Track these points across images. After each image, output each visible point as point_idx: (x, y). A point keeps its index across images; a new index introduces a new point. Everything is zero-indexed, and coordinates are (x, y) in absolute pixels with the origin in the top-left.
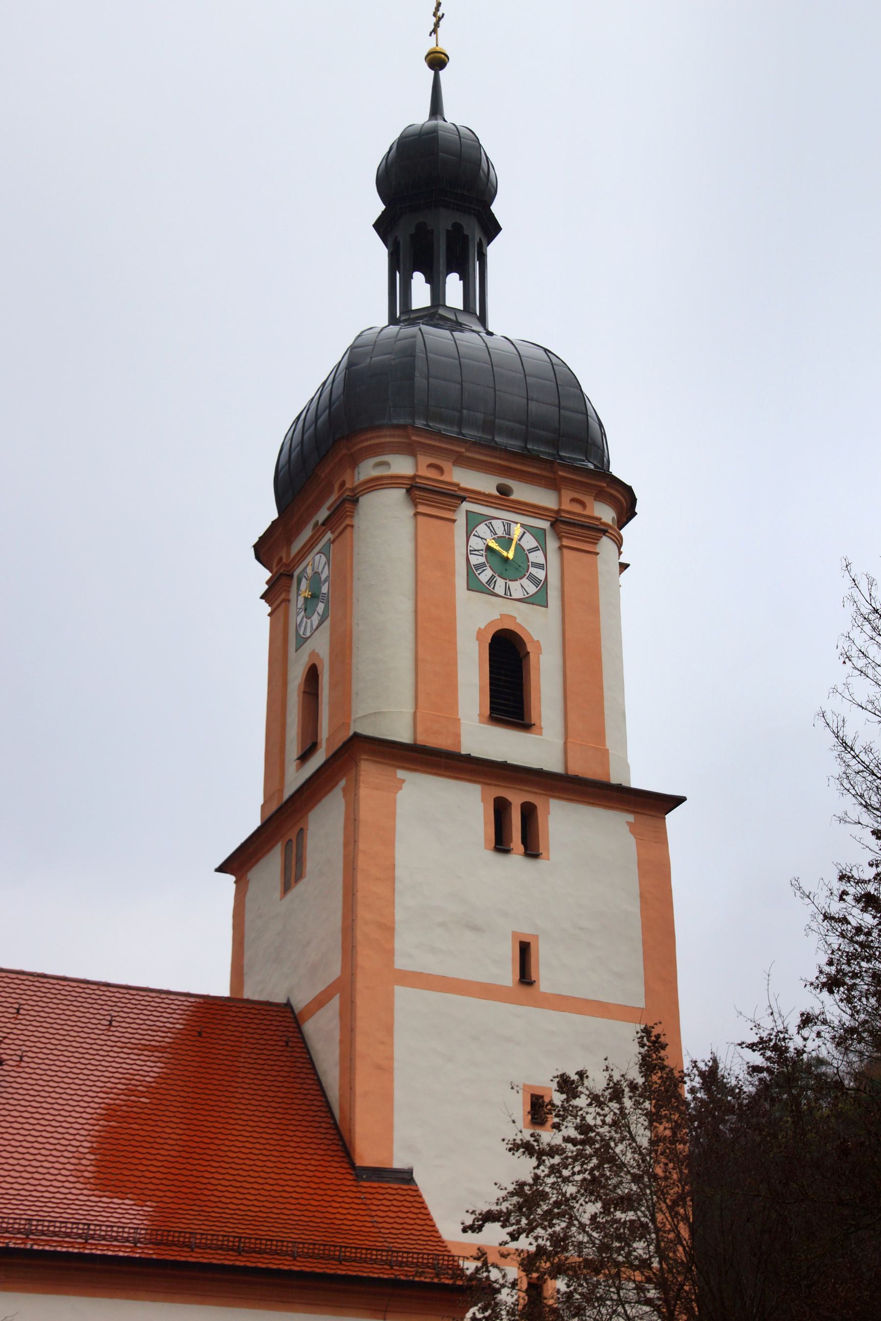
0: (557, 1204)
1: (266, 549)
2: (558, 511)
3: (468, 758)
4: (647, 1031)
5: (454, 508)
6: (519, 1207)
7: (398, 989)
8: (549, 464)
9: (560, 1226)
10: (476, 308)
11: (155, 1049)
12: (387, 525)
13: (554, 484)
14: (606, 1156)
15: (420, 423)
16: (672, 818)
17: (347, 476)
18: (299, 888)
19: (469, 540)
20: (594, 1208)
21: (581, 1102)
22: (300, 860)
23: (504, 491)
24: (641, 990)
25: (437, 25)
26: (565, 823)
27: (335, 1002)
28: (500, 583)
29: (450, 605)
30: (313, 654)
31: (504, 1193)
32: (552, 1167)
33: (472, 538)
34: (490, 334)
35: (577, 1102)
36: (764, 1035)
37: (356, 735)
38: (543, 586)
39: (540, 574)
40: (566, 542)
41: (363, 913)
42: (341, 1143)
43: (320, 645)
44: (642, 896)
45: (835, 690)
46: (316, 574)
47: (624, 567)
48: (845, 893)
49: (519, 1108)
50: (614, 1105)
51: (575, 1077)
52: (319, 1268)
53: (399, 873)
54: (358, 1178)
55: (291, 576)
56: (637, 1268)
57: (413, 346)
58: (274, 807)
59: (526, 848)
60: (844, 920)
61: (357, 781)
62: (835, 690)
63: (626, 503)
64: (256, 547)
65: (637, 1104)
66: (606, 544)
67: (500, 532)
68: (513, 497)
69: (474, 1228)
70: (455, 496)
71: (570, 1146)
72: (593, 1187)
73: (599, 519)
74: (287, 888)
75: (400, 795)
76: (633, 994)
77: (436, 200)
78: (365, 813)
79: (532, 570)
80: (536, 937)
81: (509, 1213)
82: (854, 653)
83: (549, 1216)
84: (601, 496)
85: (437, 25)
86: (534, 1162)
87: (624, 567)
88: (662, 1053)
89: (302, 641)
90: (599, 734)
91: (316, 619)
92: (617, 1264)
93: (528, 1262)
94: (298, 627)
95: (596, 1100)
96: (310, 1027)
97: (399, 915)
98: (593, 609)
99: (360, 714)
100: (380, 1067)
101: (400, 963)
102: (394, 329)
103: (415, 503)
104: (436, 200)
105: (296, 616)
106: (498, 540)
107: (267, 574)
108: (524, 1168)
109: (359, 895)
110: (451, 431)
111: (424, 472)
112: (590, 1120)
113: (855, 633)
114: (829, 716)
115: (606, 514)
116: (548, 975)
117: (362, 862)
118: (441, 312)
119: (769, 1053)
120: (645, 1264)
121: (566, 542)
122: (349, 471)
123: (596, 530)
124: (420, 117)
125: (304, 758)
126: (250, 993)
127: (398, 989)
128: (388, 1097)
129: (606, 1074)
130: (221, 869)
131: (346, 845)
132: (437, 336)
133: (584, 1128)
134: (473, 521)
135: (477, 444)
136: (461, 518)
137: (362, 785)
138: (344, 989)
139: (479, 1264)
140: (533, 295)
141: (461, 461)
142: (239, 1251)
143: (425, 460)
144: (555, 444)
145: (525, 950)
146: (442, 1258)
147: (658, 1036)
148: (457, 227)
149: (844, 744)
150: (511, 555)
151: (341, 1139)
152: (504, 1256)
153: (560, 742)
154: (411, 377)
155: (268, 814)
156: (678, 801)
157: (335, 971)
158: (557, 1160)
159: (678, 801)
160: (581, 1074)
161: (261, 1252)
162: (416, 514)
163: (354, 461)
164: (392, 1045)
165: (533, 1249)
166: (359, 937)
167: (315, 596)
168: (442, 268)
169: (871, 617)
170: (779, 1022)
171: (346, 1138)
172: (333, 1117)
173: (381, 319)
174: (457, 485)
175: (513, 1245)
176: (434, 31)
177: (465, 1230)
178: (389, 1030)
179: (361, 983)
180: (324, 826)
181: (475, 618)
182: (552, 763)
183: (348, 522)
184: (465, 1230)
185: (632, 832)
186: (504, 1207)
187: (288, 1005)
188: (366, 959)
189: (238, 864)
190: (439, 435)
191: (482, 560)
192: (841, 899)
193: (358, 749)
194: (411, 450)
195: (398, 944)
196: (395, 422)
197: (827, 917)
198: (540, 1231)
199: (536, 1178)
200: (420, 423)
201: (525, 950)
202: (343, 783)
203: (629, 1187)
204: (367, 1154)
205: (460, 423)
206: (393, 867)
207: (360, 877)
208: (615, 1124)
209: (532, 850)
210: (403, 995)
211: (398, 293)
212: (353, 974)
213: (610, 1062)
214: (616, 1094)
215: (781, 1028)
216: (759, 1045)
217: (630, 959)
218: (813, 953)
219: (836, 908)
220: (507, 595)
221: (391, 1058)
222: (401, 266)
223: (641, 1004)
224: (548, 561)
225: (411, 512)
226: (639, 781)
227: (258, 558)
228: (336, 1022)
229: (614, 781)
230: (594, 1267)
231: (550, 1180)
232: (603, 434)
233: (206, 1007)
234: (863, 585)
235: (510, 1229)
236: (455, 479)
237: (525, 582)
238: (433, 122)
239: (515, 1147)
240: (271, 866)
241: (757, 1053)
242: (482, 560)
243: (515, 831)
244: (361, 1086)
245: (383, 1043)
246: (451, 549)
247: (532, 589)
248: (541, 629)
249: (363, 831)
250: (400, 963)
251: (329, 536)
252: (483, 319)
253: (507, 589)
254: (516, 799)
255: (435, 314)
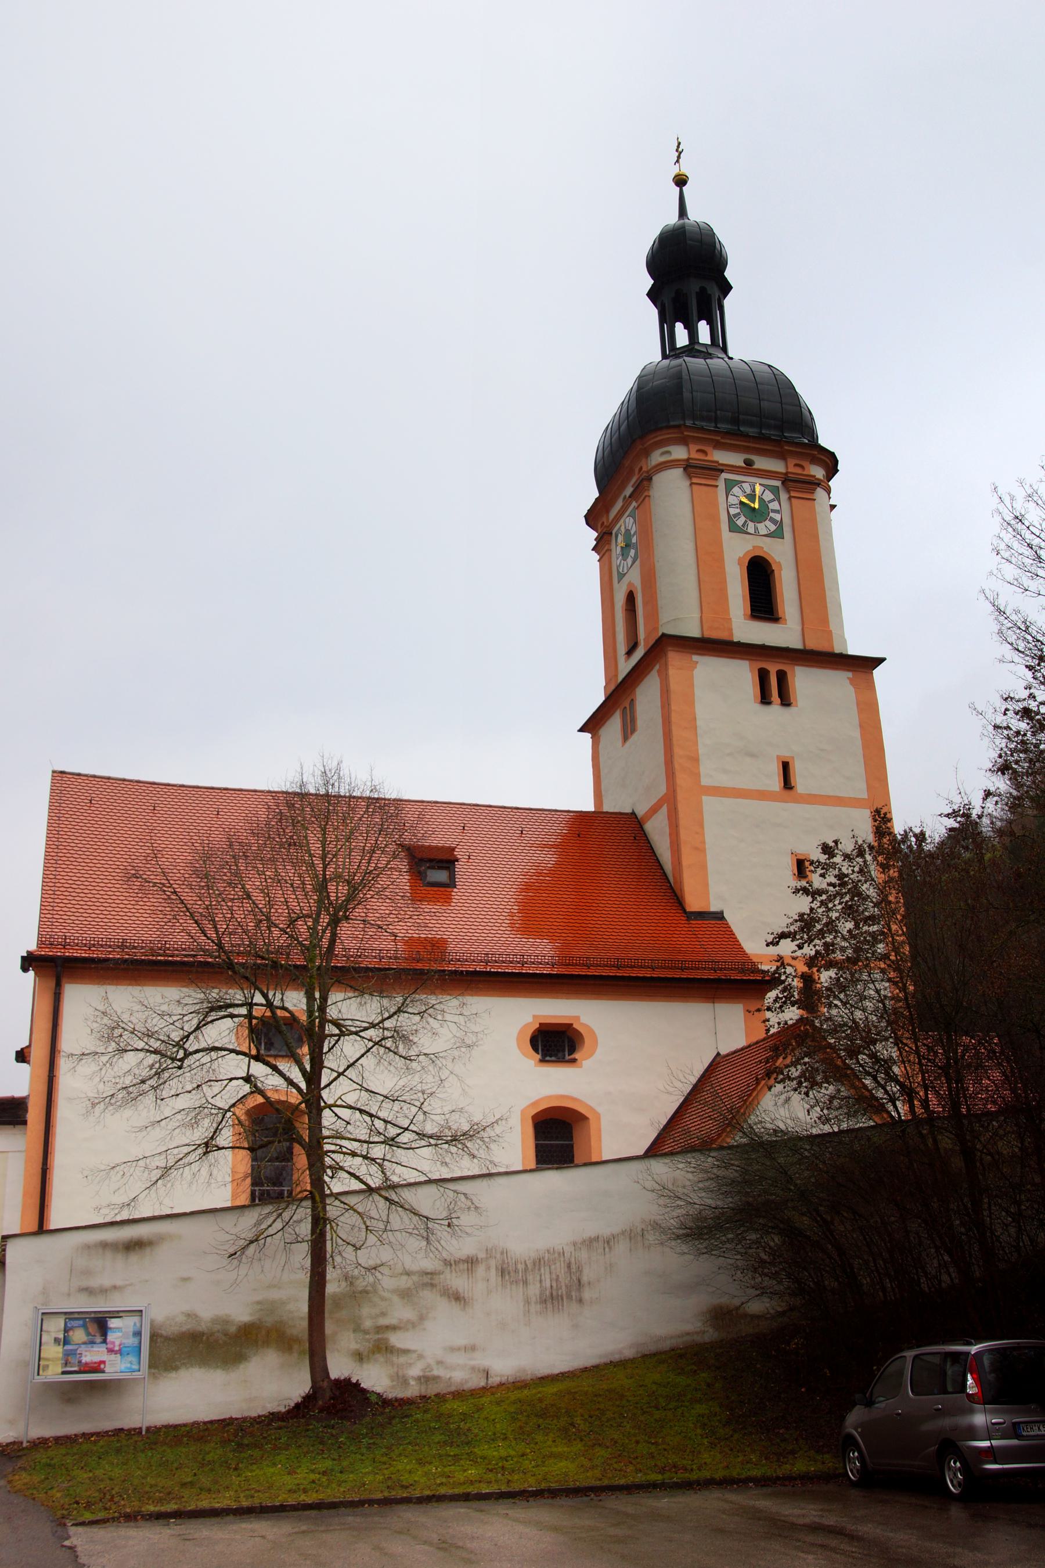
0: (826, 925)
1: (592, 518)
2: (786, 474)
3: (739, 644)
4: (878, 811)
5: (716, 478)
6: (802, 929)
7: (704, 798)
8: (778, 442)
9: (829, 939)
10: (719, 341)
11: (552, 846)
12: (672, 493)
13: (782, 456)
14: (856, 892)
15: (689, 423)
16: (878, 673)
17: (643, 463)
18: (634, 738)
19: (729, 498)
20: (850, 925)
21: (838, 859)
22: (633, 720)
23: (749, 463)
24: (864, 786)
25: (679, 157)
26: (805, 681)
27: (664, 809)
28: (751, 525)
29: (718, 543)
30: (630, 584)
31: (791, 920)
32: (822, 902)
33: (730, 497)
34: (731, 358)
35: (835, 860)
36: (956, 808)
37: (663, 635)
38: (780, 525)
39: (777, 517)
40: (793, 494)
41: (677, 751)
42: (676, 898)
43: (634, 577)
44: (861, 726)
45: (991, 573)
46: (627, 531)
47: (833, 507)
48: (1007, 709)
49: (790, 868)
50: (860, 860)
51: (832, 844)
52: (670, 974)
53: (699, 723)
54: (688, 919)
55: (611, 534)
56: (880, 960)
57: (680, 372)
58: (613, 687)
59: (782, 700)
60: (1008, 728)
61: (666, 665)
62: (991, 573)
63: (830, 463)
64: (585, 516)
65: (875, 859)
66: (820, 493)
67: (748, 491)
68: (755, 467)
69: (774, 943)
70: (716, 470)
71: (831, 888)
72: (849, 911)
73: (814, 476)
74: (625, 738)
75: (696, 672)
76: (859, 789)
77: (687, 273)
78: (673, 685)
79: (772, 515)
80: (793, 758)
81: (795, 932)
82: (1002, 546)
83: (821, 934)
84: (814, 461)
85: (679, 157)
86: (810, 899)
87: (833, 507)
88: (889, 825)
89: (621, 576)
90: (824, 620)
91: (630, 561)
92: (867, 959)
93: (811, 962)
94: (618, 567)
95: (847, 857)
96: (648, 827)
97: (702, 751)
98: (815, 537)
99: (665, 620)
100: (697, 849)
101: (705, 781)
102: (666, 362)
103: (690, 477)
104: (687, 273)
105: (616, 560)
106: (747, 496)
107: (595, 534)
108: (803, 904)
109: (674, 739)
110: (711, 426)
111: (695, 455)
112: (844, 870)
113: (1003, 534)
114: (987, 592)
115: (818, 472)
116: (802, 783)
117: (674, 718)
118: (697, 347)
119: (959, 819)
120: (885, 957)
121: (793, 494)
122: (644, 460)
123: (813, 484)
124: (672, 218)
125: (629, 653)
126: (607, 808)
127: (704, 798)
128: (704, 867)
129: (853, 840)
130: (582, 730)
131: (663, 707)
132: (696, 363)
133: (841, 876)
134: (730, 485)
135: (728, 434)
136: (721, 484)
137: (670, 667)
138: (670, 800)
139: (779, 964)
140: (755, 332)
141: (718, 446)
142: (618, 967)
143: (694, 448)
144: (781, 428)
145: (786, 766)
146: (749, 965)
147: (885, 814)
148: (703, 290)
149: (999, 610)
150: (757, 506)
151: (676, 895)
152: (794, 958)
153: (799, 628)
154: (681, 393)
155: (609, 693)
156: (880, 661)
157: (662, 789)
158: (824, 897)
159: (880, 661)
160: (836, 842)
161: (632, 967)
162: (691, 484)
163: (647, 453)
164: (703, 835)
165: (813, 953)
166: (676, 766)
167: (628, 545)
168: (695, 318)
169: (1013, 522)
170: (965, 798)
171: (679, 894)
172: (669, 882)
173: (658, 357)
174: (717, 462)
175: (799, 953)
176: (678, 161)
177: (767, 945)
178: (701, 825)
179: (681, 796)
180: (647, 697)
181: (735, 550)
182: (796, 643)
183: (646, 494)
184: (767, 945)
185: (851, 684)
186: (792, 929)
187: (633, 813)
188: (682, 780)
189: (592, 725)
190: (702, 429)
191: (738, 511)
192: (1005, 714)
193: (666, 644)
194: (684, 441)
195: (703, 770)
196: (672, 423)
197: (996, 727)
198: (817, 941)
199: (812, 909)
200: (689, 423)
201: (786, 766)
202: (657, 667)
203: (872, 910)
204: (693, 904)
205: (716, 420)
206: (695, 719)
207: (674, 728)
208: (861, 871)
209: (786, 701)
210: (709, 803)
211: (667, 339)
212: (674, 791)
213: (856, 833)
214: (861, 853)
215: (966, 802)
216: (954, 814)
217: (857, 768)
218: (988, 750)
219: (1000, 720)
220: (757, 533)
221: (704, 842)
222: (666, 320)
223: (865, 796)
224: (781, 508)
225: (688, 483)
226: (853, 650)
227: (587, 523)
228: (666, 822)
229: (837, 651)
230: (852, 961)
231: (820, 910)
232: (812, 419)
233: (580, 818)
234: (1007, 500)
235: (797, 942)
236: (715, 458)
237: (767, 523)
238: (682, 221)
239: (796, 891)
240: (614, 725)
241: (952, 820)
242: (738, 511)
243: (773, 690)
244: (685, 862)
245: (697, 833)
246: (715, 505)
247: (773, 528)
248: (781, 555)
249: (673, 696)
250: (705, 781)
251: (634, 504)
252: (725, 349)
253: (756, 529)
254: (773, 668)
255: (693, 348)
